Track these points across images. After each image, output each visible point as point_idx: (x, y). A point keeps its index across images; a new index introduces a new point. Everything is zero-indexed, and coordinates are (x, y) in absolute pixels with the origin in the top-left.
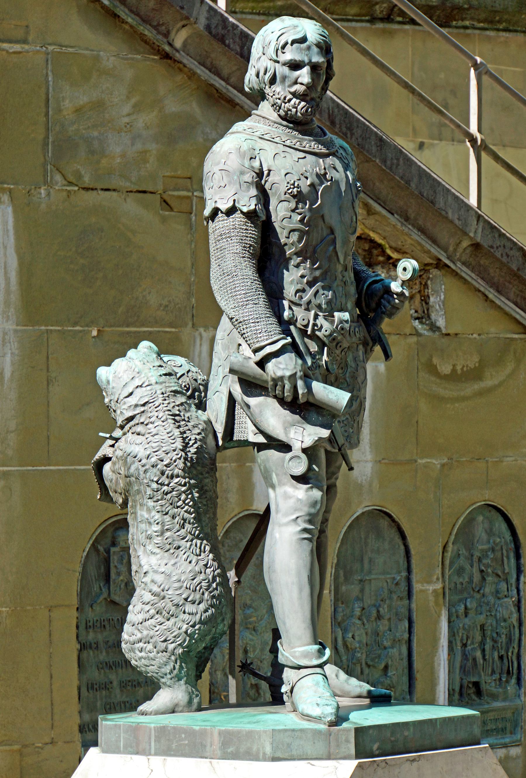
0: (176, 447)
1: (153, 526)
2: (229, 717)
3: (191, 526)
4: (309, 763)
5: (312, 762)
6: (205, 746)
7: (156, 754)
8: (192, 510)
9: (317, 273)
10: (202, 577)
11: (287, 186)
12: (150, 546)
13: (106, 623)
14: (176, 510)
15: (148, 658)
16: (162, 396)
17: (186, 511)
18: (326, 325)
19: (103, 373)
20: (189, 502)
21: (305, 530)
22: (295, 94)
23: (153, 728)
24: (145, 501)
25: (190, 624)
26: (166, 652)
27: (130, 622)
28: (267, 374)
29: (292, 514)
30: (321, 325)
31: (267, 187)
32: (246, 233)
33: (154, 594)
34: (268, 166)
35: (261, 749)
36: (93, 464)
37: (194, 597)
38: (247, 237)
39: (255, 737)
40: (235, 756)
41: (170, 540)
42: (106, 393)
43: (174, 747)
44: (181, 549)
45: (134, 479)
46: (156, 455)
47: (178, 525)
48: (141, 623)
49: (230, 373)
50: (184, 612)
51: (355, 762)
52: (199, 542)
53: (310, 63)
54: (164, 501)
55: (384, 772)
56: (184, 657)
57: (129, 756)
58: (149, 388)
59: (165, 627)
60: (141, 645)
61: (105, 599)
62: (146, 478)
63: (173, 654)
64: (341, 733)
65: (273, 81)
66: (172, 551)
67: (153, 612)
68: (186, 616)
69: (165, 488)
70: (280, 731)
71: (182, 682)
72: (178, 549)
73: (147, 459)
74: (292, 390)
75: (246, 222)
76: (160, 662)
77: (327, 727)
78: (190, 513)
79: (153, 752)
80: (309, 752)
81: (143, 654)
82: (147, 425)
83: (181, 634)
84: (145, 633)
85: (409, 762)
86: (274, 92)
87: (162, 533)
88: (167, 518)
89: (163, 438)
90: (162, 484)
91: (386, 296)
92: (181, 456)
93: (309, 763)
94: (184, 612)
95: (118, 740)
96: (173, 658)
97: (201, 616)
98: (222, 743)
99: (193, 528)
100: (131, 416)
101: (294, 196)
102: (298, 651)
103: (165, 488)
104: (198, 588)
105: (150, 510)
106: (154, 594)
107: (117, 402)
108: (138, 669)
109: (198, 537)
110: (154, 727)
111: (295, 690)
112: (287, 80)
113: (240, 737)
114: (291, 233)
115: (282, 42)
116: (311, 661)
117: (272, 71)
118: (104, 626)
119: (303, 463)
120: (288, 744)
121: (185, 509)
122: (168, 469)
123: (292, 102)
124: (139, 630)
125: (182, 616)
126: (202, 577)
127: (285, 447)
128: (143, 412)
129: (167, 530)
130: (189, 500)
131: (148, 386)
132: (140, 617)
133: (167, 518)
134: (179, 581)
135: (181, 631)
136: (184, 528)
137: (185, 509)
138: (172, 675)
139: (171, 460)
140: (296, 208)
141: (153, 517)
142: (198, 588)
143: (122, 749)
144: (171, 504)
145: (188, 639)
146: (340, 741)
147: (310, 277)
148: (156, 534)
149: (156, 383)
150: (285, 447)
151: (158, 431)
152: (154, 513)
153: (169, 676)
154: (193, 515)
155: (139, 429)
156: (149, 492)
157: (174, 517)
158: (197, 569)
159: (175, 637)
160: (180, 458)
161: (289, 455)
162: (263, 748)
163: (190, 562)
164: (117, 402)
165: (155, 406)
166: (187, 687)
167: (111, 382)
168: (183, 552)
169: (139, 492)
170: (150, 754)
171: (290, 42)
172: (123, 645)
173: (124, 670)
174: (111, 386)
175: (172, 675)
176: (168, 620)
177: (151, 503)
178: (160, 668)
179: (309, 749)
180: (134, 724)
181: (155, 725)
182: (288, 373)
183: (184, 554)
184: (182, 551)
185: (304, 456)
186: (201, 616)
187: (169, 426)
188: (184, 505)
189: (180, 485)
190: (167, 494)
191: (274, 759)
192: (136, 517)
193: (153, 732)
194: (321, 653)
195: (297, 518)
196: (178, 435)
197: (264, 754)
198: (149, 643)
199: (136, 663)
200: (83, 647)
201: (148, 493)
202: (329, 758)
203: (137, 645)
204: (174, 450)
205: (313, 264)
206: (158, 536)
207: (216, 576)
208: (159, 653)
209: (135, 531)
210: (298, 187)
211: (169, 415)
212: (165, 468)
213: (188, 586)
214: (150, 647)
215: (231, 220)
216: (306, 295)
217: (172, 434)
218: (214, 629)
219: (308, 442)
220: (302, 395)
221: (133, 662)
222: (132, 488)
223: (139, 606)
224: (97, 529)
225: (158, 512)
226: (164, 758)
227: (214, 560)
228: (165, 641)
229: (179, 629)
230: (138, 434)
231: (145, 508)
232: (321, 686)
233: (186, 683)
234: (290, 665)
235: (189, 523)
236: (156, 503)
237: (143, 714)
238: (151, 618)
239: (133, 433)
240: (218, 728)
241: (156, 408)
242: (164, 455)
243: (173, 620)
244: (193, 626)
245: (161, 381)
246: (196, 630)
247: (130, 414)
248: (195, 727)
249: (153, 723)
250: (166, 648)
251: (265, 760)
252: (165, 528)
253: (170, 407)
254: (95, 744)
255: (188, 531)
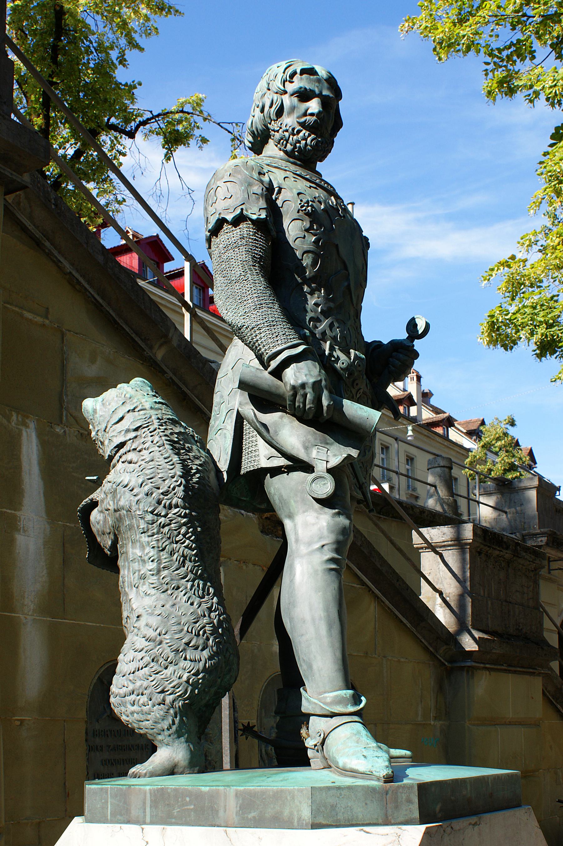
0: (175, 474)
1: (147, 564)
2: (243, 776)
3: (192, 564)
4: (362, 830)
5: (366, 829)
6: (217, 811)
7: (152, 823)
8: (194, 545)
9: (332, 305)
10: (206, 620)
11: (300, 204)
12: (144, 587)
13: (109, 733)
14: (175, 545)
15: (141, 712)
16: (158, 421)
17: (186, 547)
18: (343, 357)
19: (88, 404)
20: (191, 537)
21: (332, 560)
22: (303, 125)
23: (148, 792)
24: (138, 536)
25: (192, 672)
26: (164, 704)
27: (120, 673)
28: (285, 384)
29: (318, 542)
30: (338, 356)
31: (279, 203)
32: (255, 243)
33: (149, 640)
34: (278, 183)
35: (295, 813)
36: (79, 511)
37: (196, 642)
38: (257, 247)
39: (287, 798)
40: (259, 823)
41: (168, 579)
42: (93, 425)
43: (175, 814)
44: (180, 590)
45: (125, 512)
46: (151, 483)
47: (177, 562)
48: (133, 673)
49: (239, 387)
50: (185, 659)
51: (423, 828)
52: (201, 583)
53: (320, 96)
54: (160, 535)
55: (450, 840)
56: (184, 711)
57: (119, 825)
58: (142, 412)
59: (162, 677)
60: (133, 697)
61: (108, 716)
62: (139, 510)
63: (173, 707)
64: (401, 790)
65: (280, 112)
66: (169, 592)
67: (147, 659)
68: (188, 664)
69: (162, 520)
70: (321, 789)
71: (182, 739)
72: (176, 589)
73: (141, 487)
74: (316, 402)
75: (255, 233)
76: (156, 716)
77: (381, 784)
78: (191, 549)
79: (148, 819)
80: (360, 816)
81: (135, 708)
82: (140, 451)
83: (182, 684)
84: (138, 683)
85: (471, 826)
86: (281, 124)
87: (159, 572)
88: (164, 555)
89: (160, 463)
90: (158, 515)
91: (394, 354)
92: (181, 482)
93: (362, 830)
94: (185, 659)
95: (104, 807)
96: (172, 711)
97: (206, 663)
98: (240, 807)
99: (195, 566)
100: (121, 443)
101: (308, 214)
102: (329, 696)
103: (162, 520)
104: (201, 633)
105: (143, 546)
106: (149, 640)
107: (105, 431)
108: (130, 726)
109: (201, 577)
110: (150, 790)
111: (328, 741)
112: (295, 111)
113: (264, 799)
114: (305, 255)
115: (290, 71)
116: (347, 708)
117: (279, 102)
118: (107, 735)
119: (329, 483)
120: (332, 806)
121: (185, 544)
122: (166, 497)
123: (301, 134)
124: (130, 680)
125: (182, 664)
126: (206, 620)
127: (308, 468)
128: (136, 437)
129: (164, 568)
130: (190, 534)
131: (141, 410)
132: (132, 667)
133: (164, 555)
134: (180, 624)
135: (181, 680)
136: (184, 567)
137: (185, 544)
138: (171, 731)
139: (169, 487)
140: (311, 228)
141: (147, 554)
142: (201, 633)
143: (109, 817)
144: (169, 538)
145: (190, 689)
146: (399, 801)
147: (324, 307)
148: (151, 573)
149: (151, 408)
150: (308, 468)
151: (153, 456)
152: (147, 550)
153: (167, 733)
154: (195, 551)
155: (131, 456)
156: (143, 525)
157: (172, 554)
158: (199, 612)
159: (174, 687)
160: (179, 486)
161: (313, 475)
162: (298, 811)
163: (192, 604)
164: (105, 431)
165: (150, 430)
166: (189, 745)
167: (98, 411)
168: (184, 592)
169: (131, 527)
170: (145, 823)
171: (298, 71)
172: (112, 700)
173: (122, 766)
174: (98, 416)
175: (171, 731)
176: (166, 668)
177: (144, 538)
178: (156, 722)
179: (359, 811)
180: (124, 787)
181: (151, 787)
182: (312, 380)
183: (184, 595)
184: (182, 591)
185: (328, 476)
186: (206, 663)
187: (167, 451)
188: (184, 539)
189: (180, 516)
190: (164, 527)
191: (315, 826)
192: (127, 557)
193: (148, 795)
194: (356, 700)
195: (323, 546)
196: (177, 460)
197: (299, 819)
198: (142, 694)
199: (127, 719)
200: (91, 749)
201: (142, 527)
202: (387, 823)
203: (128, 698)
204: (173, 477)
205: (327, 293)
206: (153, 575)
207: (222, 621)
208: (155, 706)
209: (126, 572)
210: (312, 206)
211: (166, 440)
212: (162, 496)
213: (190, 630)
214: (144, 699)
215: (238, 231)
216: (321, 325)
217: (170, 459)
218: (219, 680)
219: (334, 461)
220: (327, 407)
221: (124, 718)
222: (123, 524)
223: (131, 654)
224: (102, 667)
225: (153, 547)
226: (163, 826)
227: (218, 604)
228: (163, 692)
229: (179, 678)
230: (130, 462)
231: (138, 544)
232: (363, 736)
233: (186, 742)
234: (318, 713)
235: (190, 561)
236: (150, 538)
237: (135, 776)
238: (146, 667)
239: (123, 462)
240: (235, 788)
241: (151, 432)
242: (160, 481)
243: (171, 669)
244: (197, 674)
245: (156, 407)
246: (199, 679)
247: (121, 439)
248: (203, 789)
249: (148, 785)
250: (164, 700)
251: (301, 827)
252: (162, 566)
253: (168, 432)
254: (81, 813)
255: (189, 569)
